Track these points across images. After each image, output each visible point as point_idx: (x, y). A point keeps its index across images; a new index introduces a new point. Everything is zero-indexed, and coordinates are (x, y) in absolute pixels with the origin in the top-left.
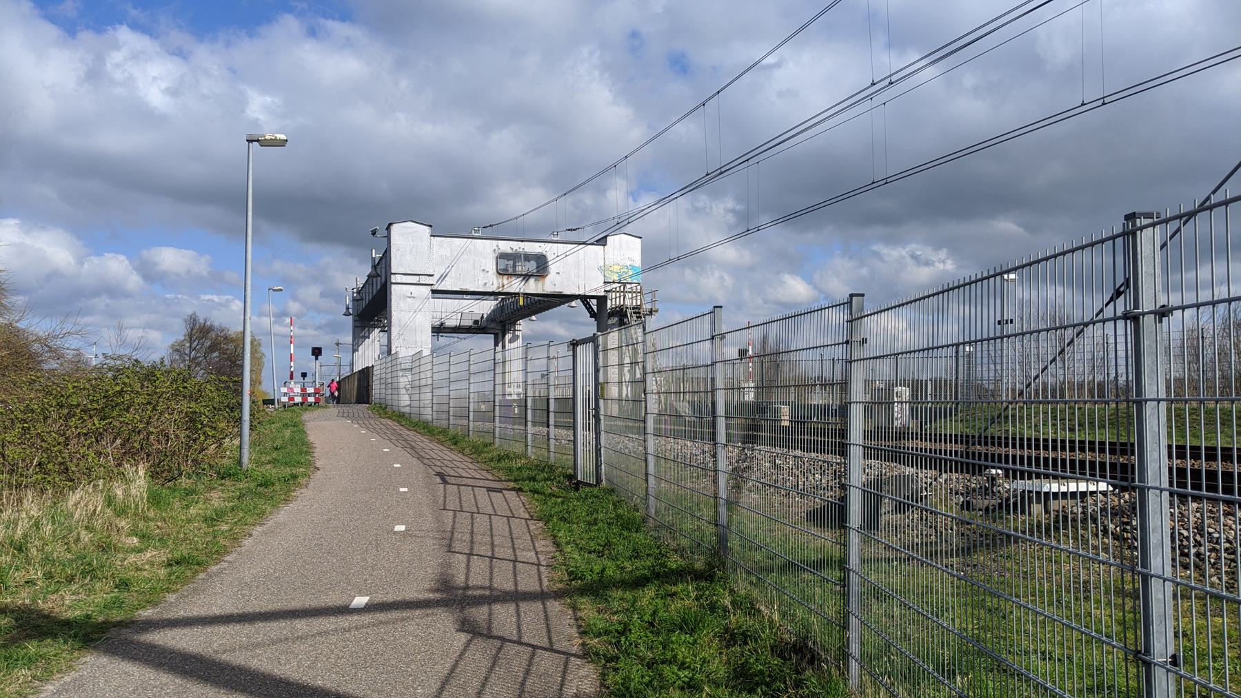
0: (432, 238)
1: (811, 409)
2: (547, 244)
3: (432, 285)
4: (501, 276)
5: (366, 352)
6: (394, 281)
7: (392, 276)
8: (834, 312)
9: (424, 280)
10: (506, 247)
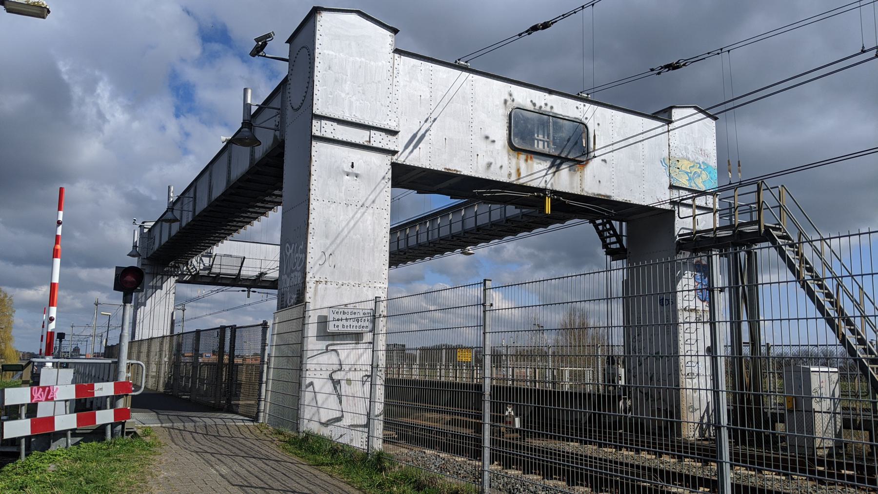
0: (397, 56)
1: (451, 359)
2: (588, 105)
3: (394, 153)
4: (516, 154)
5: (157, 308)
6: (318, 134)
7: (314, 122)
8: (510, 292)
9: (379, 140)
10: (524, 97)
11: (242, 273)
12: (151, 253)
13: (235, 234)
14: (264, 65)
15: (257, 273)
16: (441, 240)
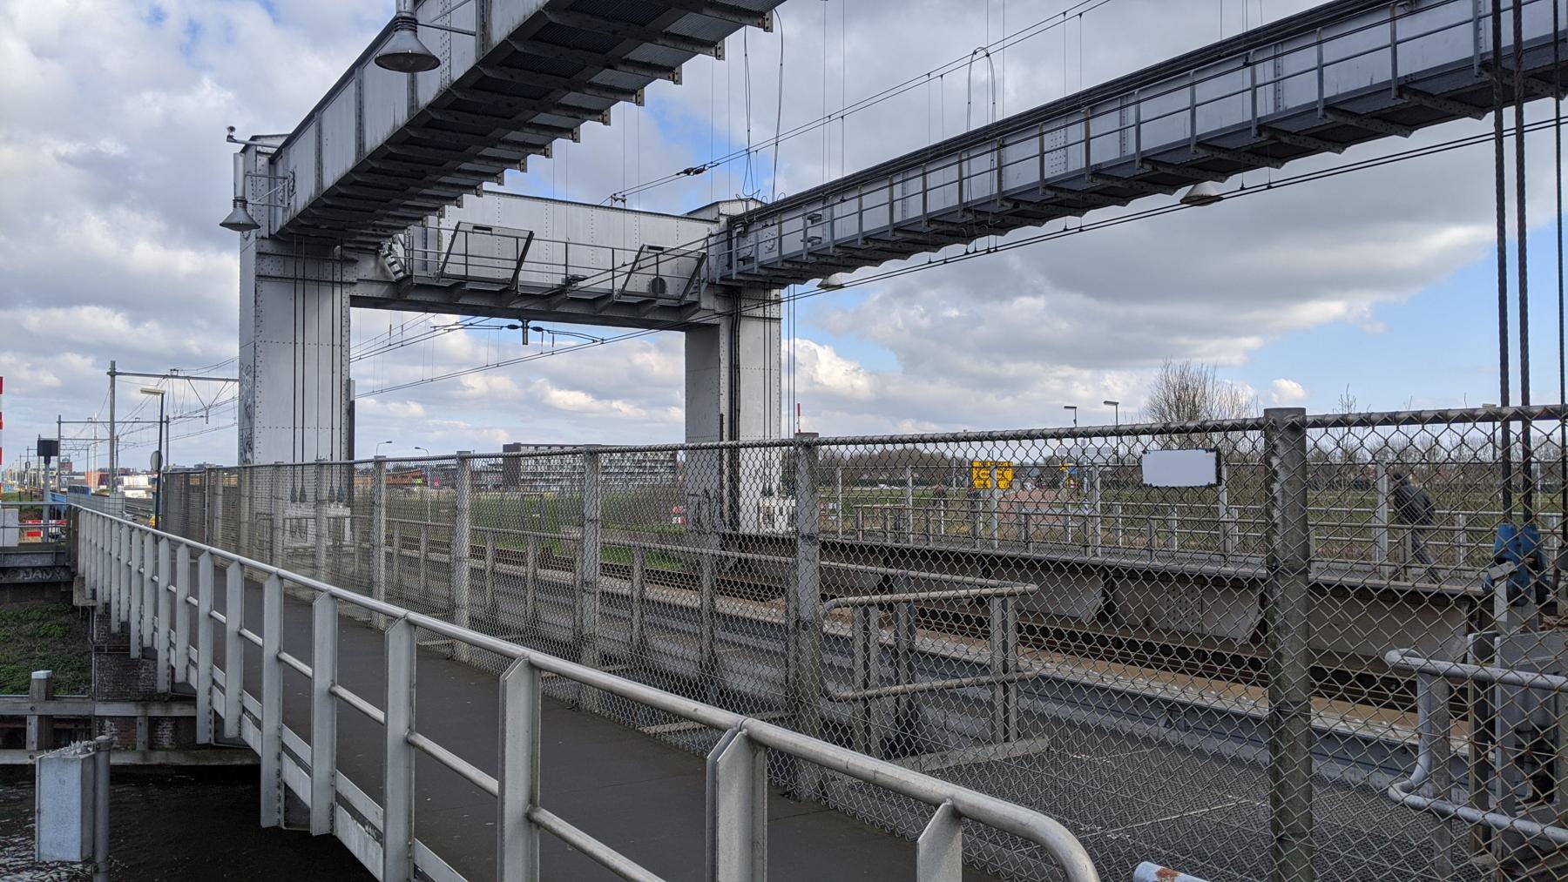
11: (522, 277)
12: (281, 220)
13: (510, 174)
14: (187, 50)
15: (558, 280)
16: (895, 230)
